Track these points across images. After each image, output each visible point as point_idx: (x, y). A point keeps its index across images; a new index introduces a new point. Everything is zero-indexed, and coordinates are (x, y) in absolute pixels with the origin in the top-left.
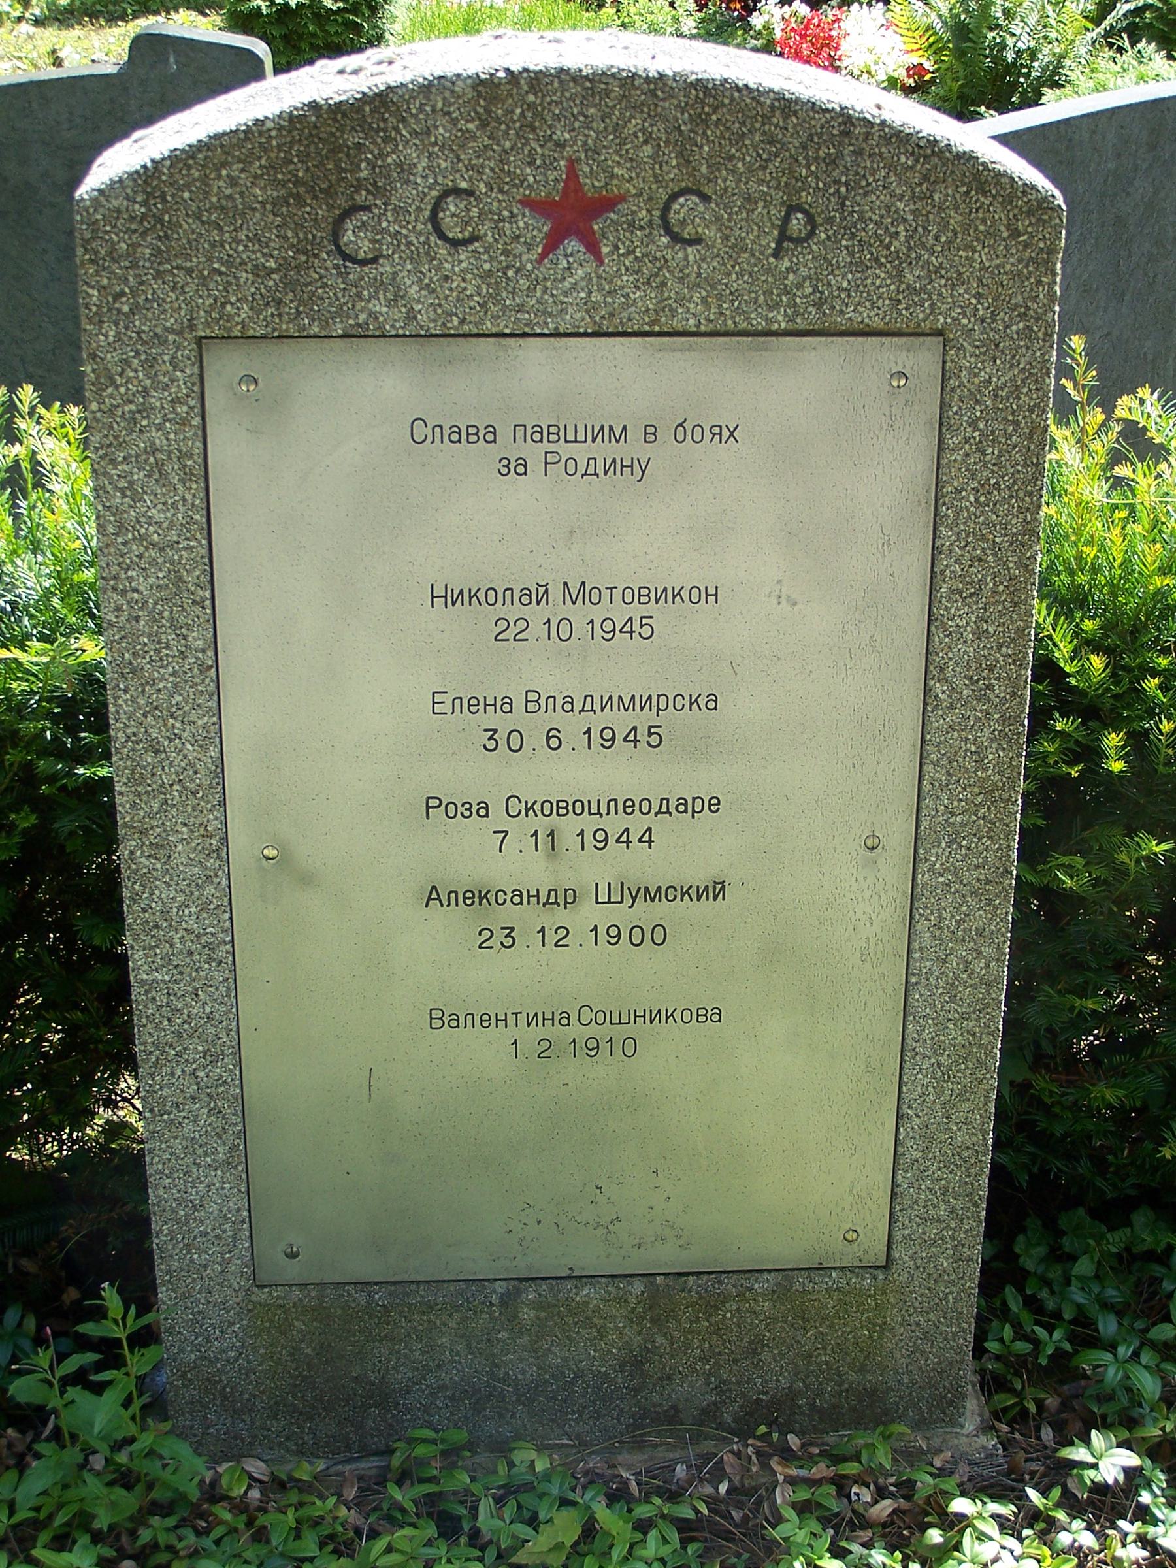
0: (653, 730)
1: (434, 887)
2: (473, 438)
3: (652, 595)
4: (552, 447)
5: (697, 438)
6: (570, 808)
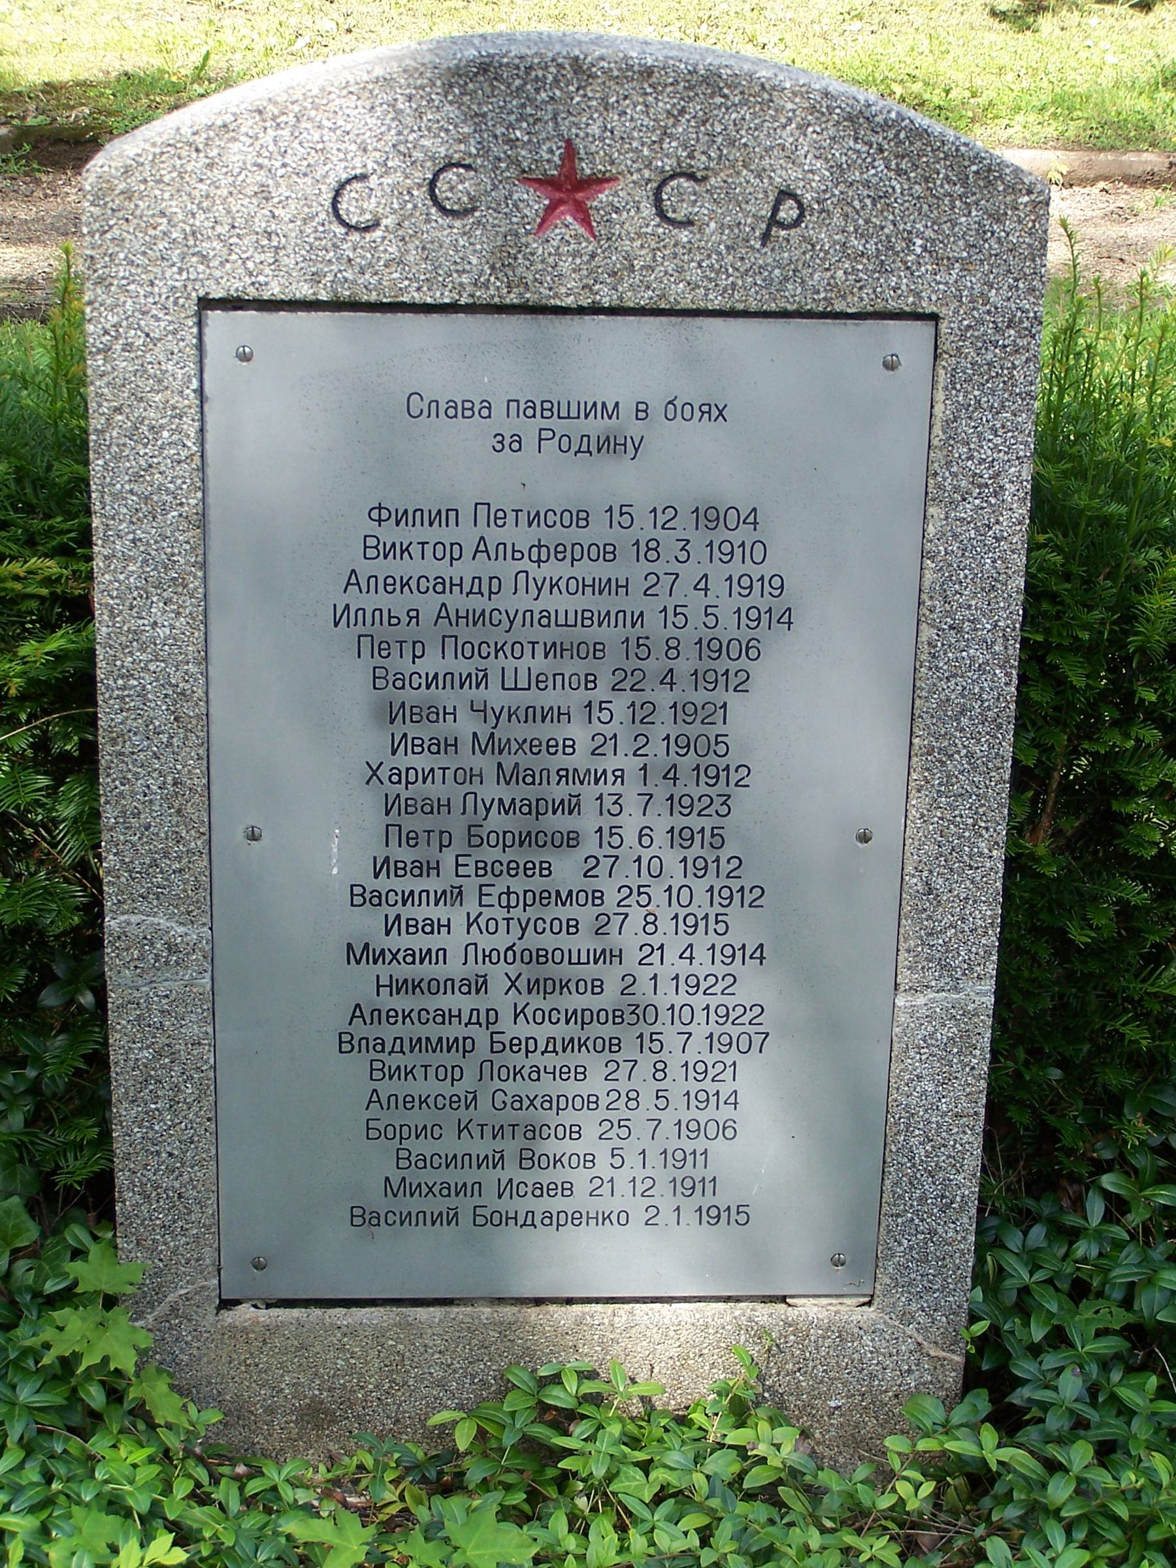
0: (679, 610)
1: (353, 571)
2: (468, 413)
3: (595, 618)
4: (545, 423)
5: (687, 415)
6: (489, 868)
